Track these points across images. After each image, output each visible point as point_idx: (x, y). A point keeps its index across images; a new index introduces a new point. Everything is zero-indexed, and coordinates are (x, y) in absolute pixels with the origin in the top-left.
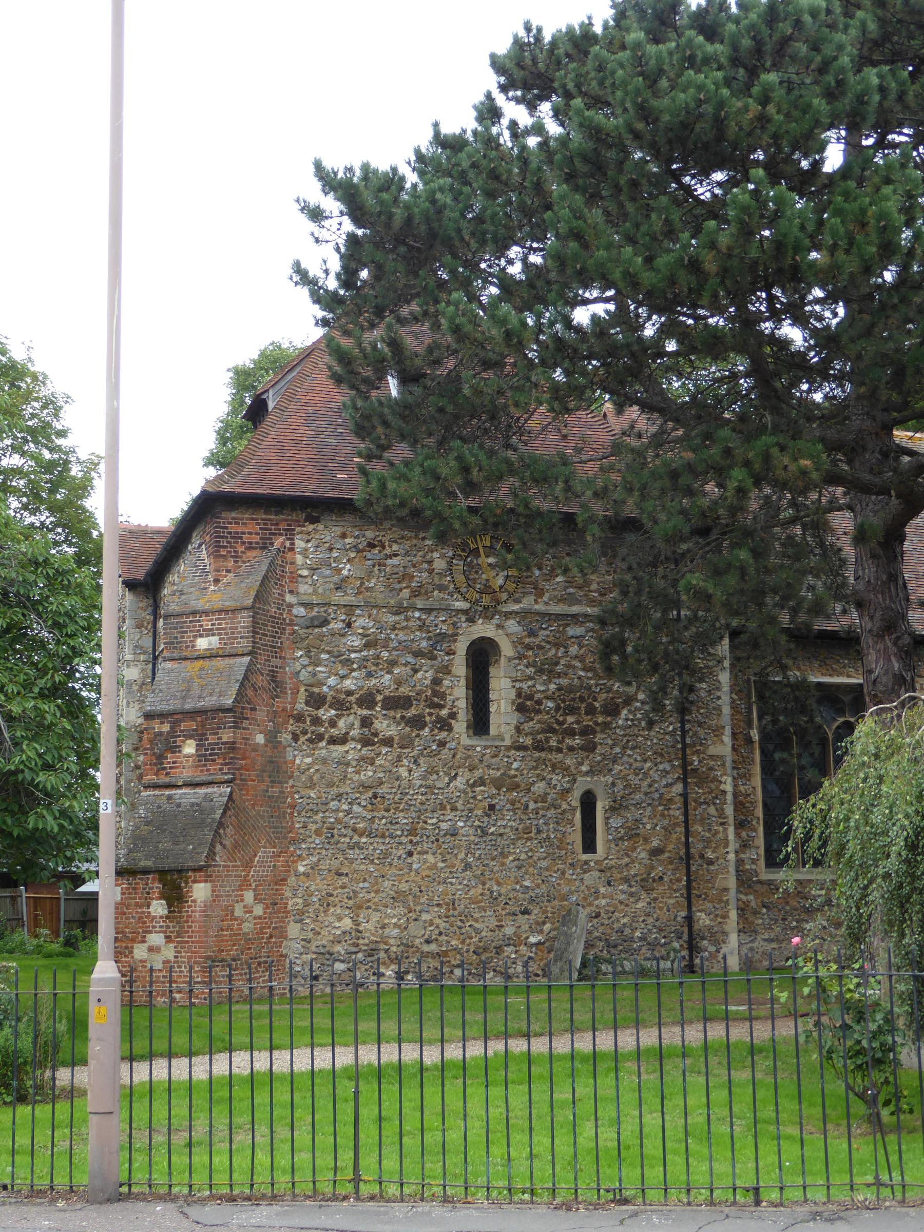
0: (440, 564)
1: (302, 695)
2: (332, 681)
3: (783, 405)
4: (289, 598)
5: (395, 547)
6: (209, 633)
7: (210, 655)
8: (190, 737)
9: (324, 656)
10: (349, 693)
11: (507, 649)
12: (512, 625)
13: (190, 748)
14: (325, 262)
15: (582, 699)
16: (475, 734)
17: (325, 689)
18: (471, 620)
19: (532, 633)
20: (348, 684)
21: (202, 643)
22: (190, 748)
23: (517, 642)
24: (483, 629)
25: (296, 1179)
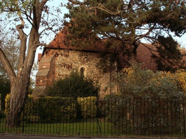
0: (77, 57)
1: (57, 74)
2: (62, 73)
3: (33, 78)
4: (56, 61)
5: (71, 55)
6: (45, 66)
7: (45, 69)
8: (41, 79)
9: (61, 69)
10: (64, 74)
11: (86, 69)
12: (87, 66)
13: (41, 81)
14: (61, 13)
15: (96, 76)
16: (177, 44)
17: (61, 74)
18: (81, 65)
19: (90, 67)
20: (64, 73)
21: (44, 67)
22: (41, 81)
23: (88, 68)
24: (83, 66)
25: (70, 132)
